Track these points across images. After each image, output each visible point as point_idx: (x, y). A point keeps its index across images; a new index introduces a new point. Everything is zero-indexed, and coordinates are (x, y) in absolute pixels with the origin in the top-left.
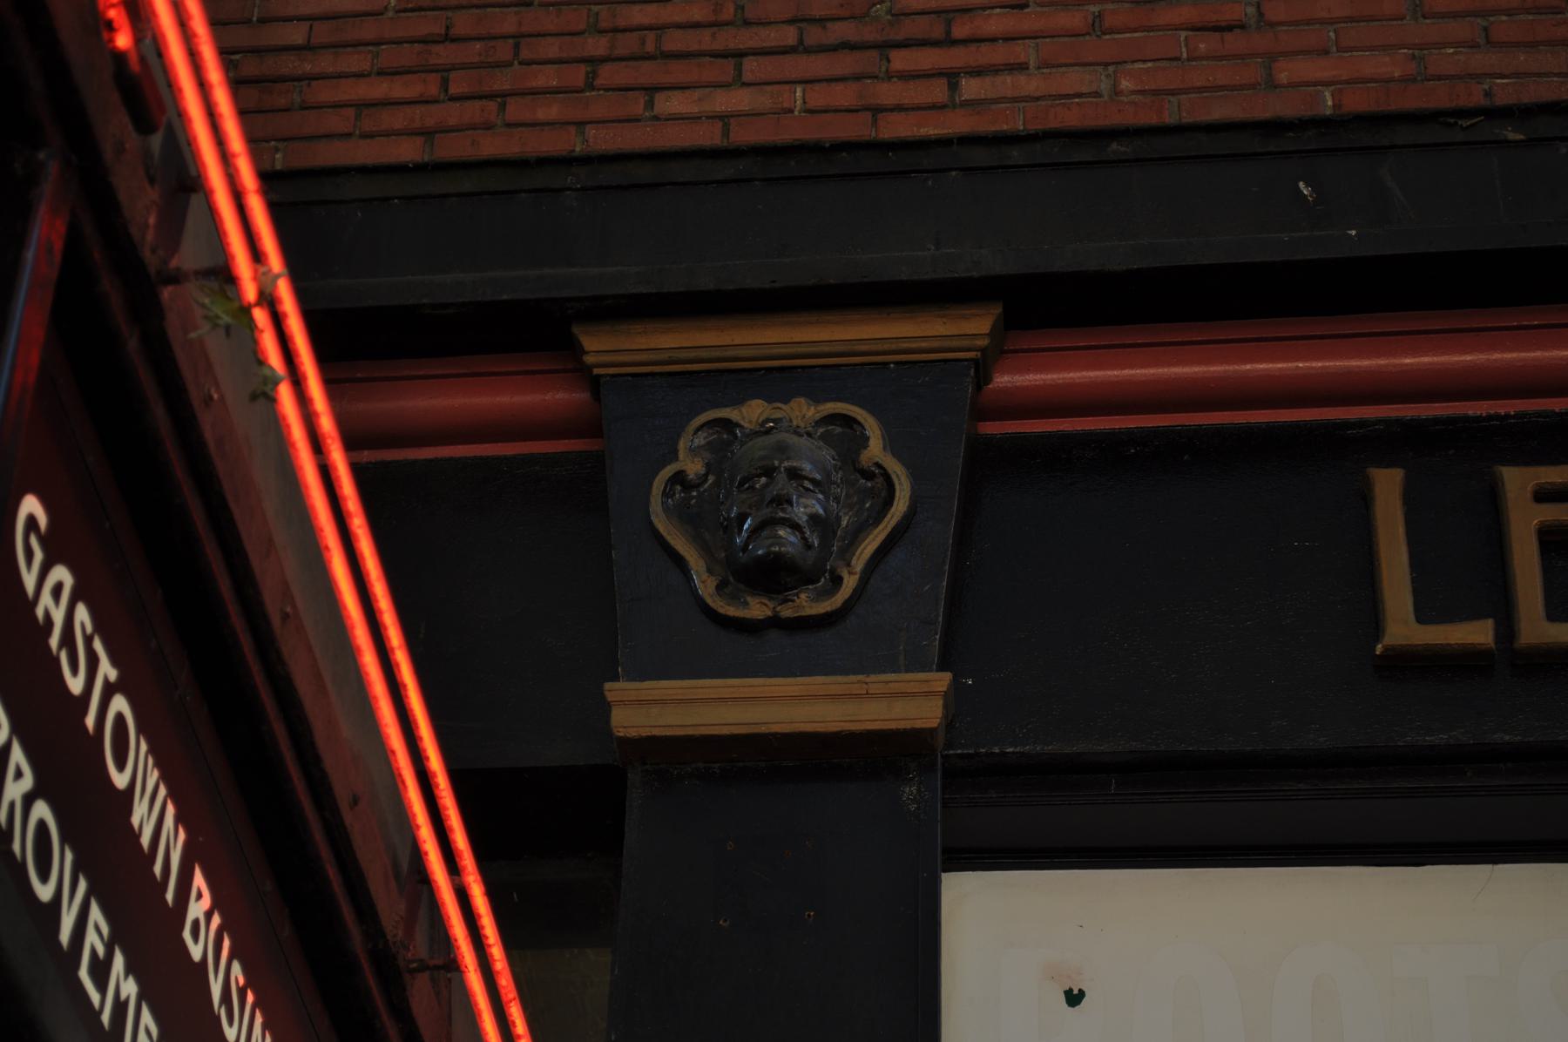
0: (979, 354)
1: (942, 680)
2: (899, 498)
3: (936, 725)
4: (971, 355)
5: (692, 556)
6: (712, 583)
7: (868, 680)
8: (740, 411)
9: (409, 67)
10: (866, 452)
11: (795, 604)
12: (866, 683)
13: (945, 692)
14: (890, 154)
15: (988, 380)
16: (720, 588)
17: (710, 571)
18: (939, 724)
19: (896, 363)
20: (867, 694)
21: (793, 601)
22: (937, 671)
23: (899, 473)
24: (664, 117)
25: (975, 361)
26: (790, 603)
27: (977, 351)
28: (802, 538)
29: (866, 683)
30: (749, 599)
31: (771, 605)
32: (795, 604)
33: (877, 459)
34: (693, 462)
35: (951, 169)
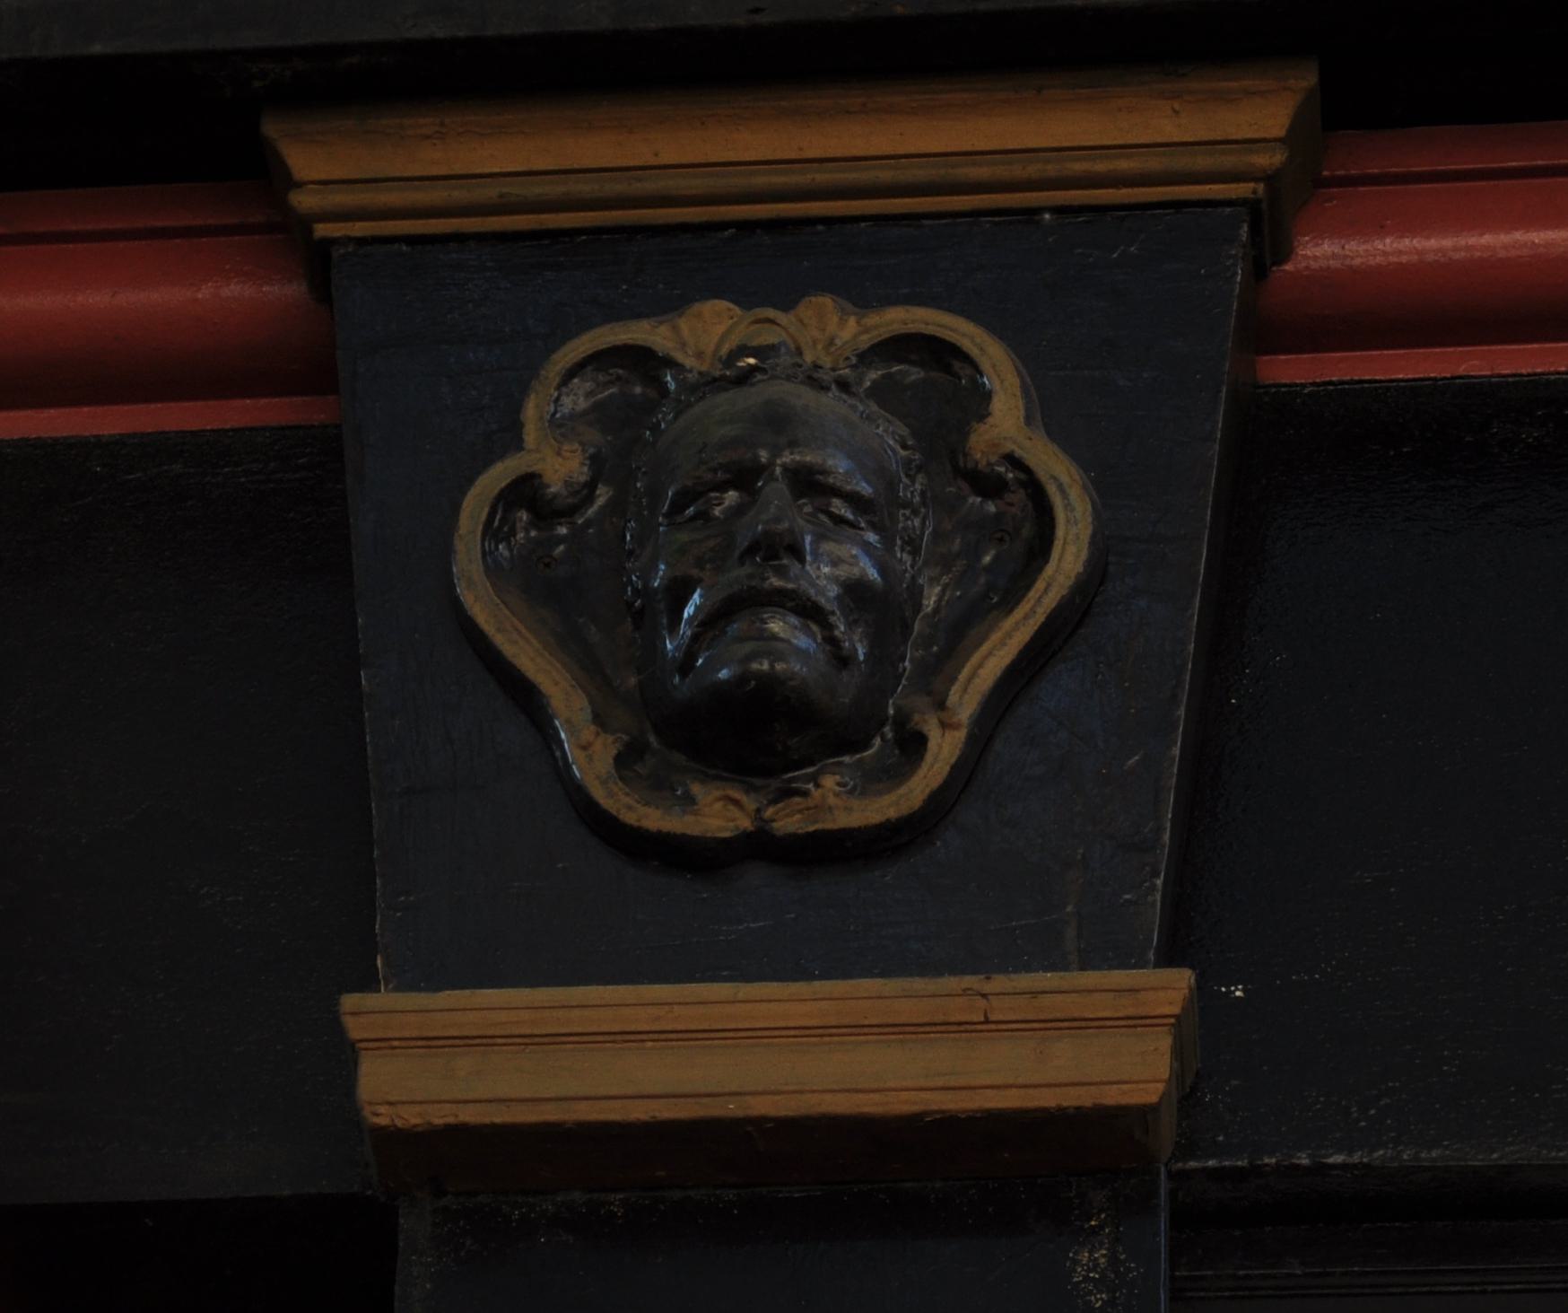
0: (1261, 187)
1: (1181, 980)
3: (1154, 1099)
7: (988, 988)
15: (1283, 252)
19: (1059, 210)
20: (987, 1021)
21: (805, 794)
23: (1065, 479)
25: (1252, 206)
26: (797, 799)
27: (1256, 180)
30: (696, 789)
31: (750, 803)
32: (810, 802)
33: (1009, 447)
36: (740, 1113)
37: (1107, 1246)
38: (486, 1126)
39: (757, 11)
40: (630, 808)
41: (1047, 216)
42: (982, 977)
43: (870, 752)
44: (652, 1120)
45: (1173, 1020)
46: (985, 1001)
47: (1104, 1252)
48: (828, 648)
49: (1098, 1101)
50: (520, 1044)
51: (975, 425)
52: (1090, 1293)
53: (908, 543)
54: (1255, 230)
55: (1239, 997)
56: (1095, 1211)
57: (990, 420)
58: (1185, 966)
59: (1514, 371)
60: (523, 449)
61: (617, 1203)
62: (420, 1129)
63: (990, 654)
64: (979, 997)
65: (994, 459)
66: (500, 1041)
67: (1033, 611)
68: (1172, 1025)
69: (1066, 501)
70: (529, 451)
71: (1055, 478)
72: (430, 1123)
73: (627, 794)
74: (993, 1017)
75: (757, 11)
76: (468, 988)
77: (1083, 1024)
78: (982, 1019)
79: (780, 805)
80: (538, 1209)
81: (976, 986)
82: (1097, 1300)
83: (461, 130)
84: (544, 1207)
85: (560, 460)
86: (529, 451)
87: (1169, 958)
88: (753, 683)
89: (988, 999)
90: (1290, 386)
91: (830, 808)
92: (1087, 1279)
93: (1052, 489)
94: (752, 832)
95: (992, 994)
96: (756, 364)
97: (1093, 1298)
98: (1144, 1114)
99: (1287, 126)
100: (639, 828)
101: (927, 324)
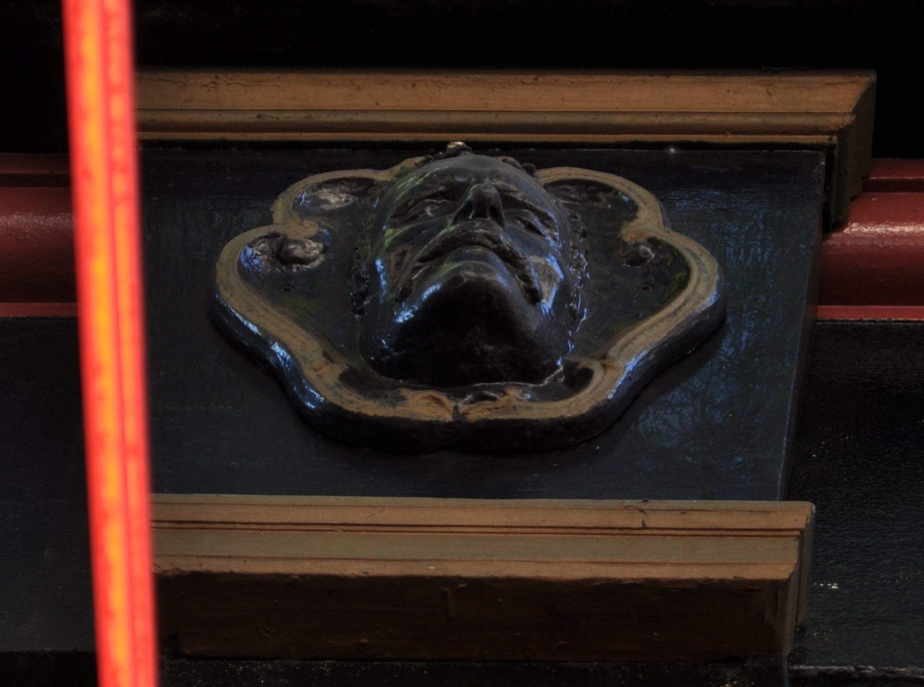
0: (835, 138)
2: (699, 280)
3: (785, 576)
4: (823, 139)
7: (645, 506)
10: (632, 224)
11: (498, 404)
12: (642, 511)
13: (802, 531)
15: (840, 225)
16: (350, 379)
18: (791, 575)
19: (680, 145)
21: (493, 399)
22: (780, 500)
24: (668, 565)
26: (488, 402)
27: (831, 133)
29: (642, 511)
30: (404, 392)
31: (450, 404)
32: (498, 404)
33: (651, 235)
34: (301, 224)
40: (352, 402)
41: (672, 150)
42: (641, 500)
46: (643, 514)
48: (522, 283)
51: (625, 223)
53: (580, 266)
58: (806, 500)
60: (272, 223)
61: (326, 665)
62: (170, 574)
64: (638, 511)
65: (641, 240)
66: (238, 526)
67: (674, 313)
68: (798, 537)
69: (698, 261)
74: (648, 525)
76: (214, 493)
78: (641, 526)
79: (472, 406)
85: (302, 228)
86: (277, 224)
87: (792, 493)
88: (470, 217)
89: (645, 513)
90: (842, 321)
91: (515, 407)
93: (687, 255)
94: (450, 423)
96: (463, 145)
98: (777, 587)
99: (854, 106)
100: (359, 414)
101: (587, 176)
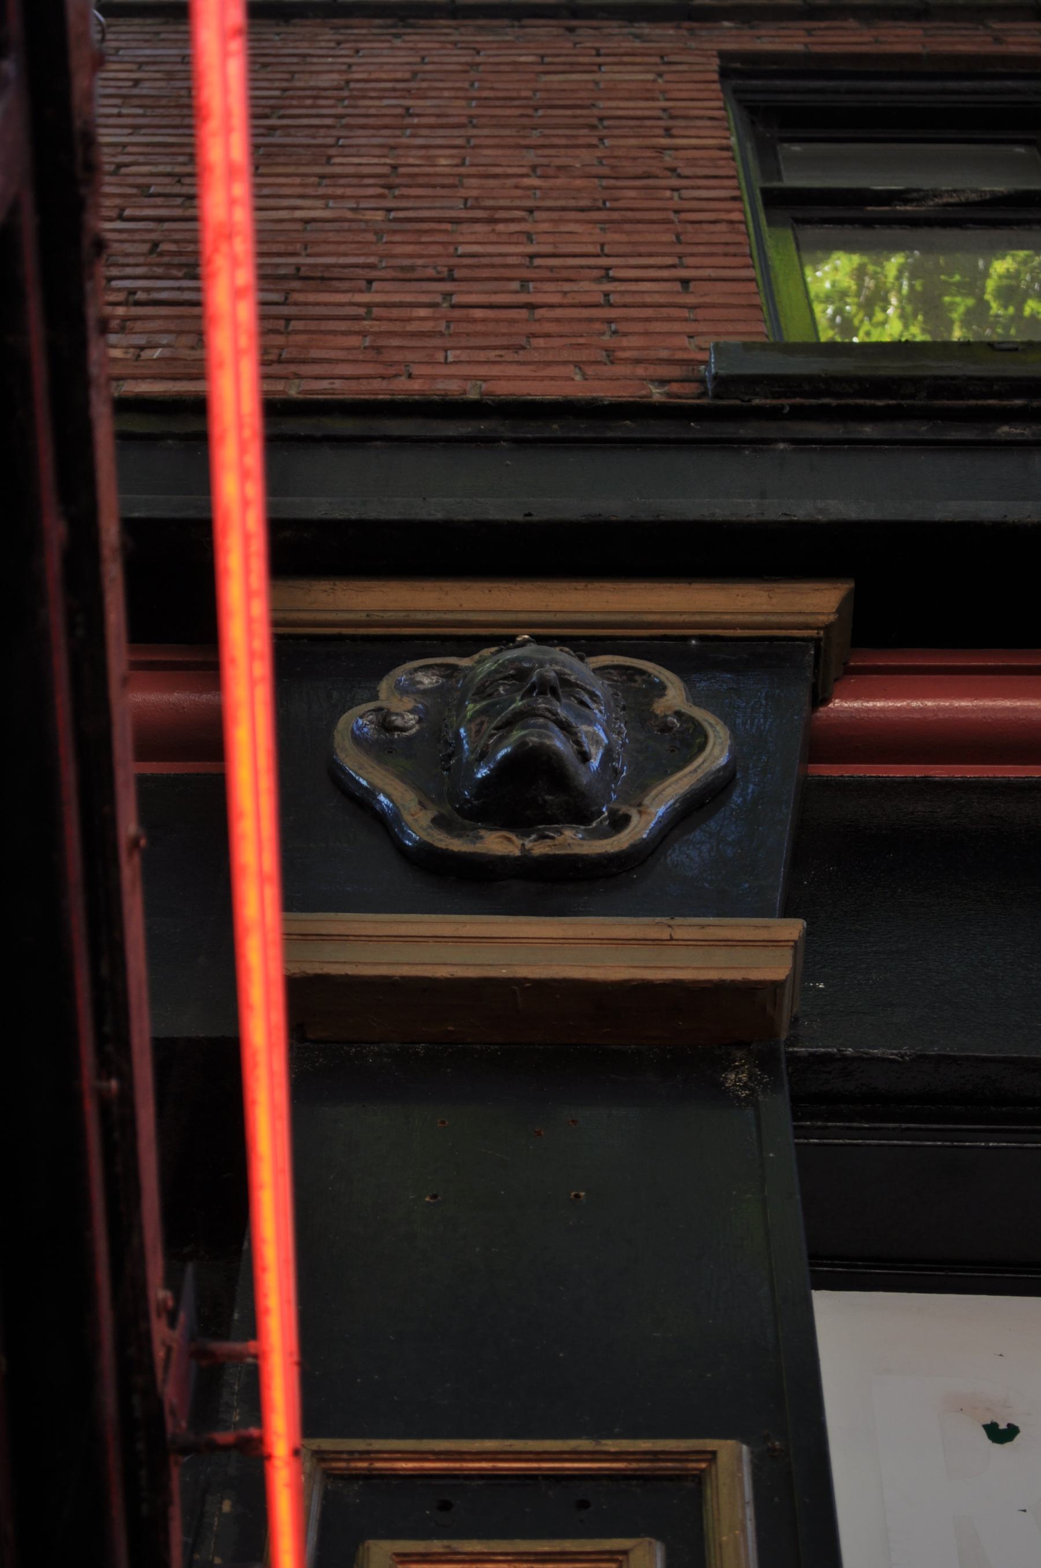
0: (822, 632)
1: (793, 929)
3: (782, 977)
4: (813, 633)
5: (396, 789)
6: (425, 818)
7: (671, 922)
8: (713, 71)
9: (513, 26)
12: (670, 926)
13: (795, 942)
14: (692, 424)
15: (826, 701)
17: (423, 805)
19: (701, 638)
20: (671, 939)
21: (553, 838)
23: (713, 721)
25: (817, 641)
26: (548, 840)
27: (818, 628)
28: (576, 734)
30: (482, 832)
31: (518, 842)
32: (556, 842)
33: (677, 708)
34: (401, 700)
35: (776, 441)
36: (511, 975)
37: (747, 1073)
38: (341, 976)
39: (530, 515)
40: (441, 840)
41: (694, 642)
42: (669, 918)
43: (590, 827)
44: (451, 976)
45: (792, 944)
46: (670, 929)
47: (745, 1075)
48: (575, 747)
49: (745, 977)
50: (366, 941)
51: (656, 699)
52: (738, 1091)
54: (818, 650)
55: (822, 988)
56: (738, 1059)
57: (666, 698)
59: (963, 776)
62: (297, 976)
63: (669, 786)
65: (669, 713)
66: (351, 938)
68: (792, 946)
69: (714, 729)
70: (382, 700)
71: (706, 721)
72: (304, 972)
73: (438, 834)
74: (675, 937)
75: (530, 515)
77: (734, 943)
78: (669, 938)
80: (368, 1049)
81: (664, 922)
82: (743, 1094)
83: (345, 588)
84: (372, 1048)
85: (402, 703)
87: (788, 911)
89: (672, 928)
90: (827, 777)
92: (734, 1085)
95: (674, 925)
97: (739, 1093)
98: (776, 986)
99: (837, 607)
